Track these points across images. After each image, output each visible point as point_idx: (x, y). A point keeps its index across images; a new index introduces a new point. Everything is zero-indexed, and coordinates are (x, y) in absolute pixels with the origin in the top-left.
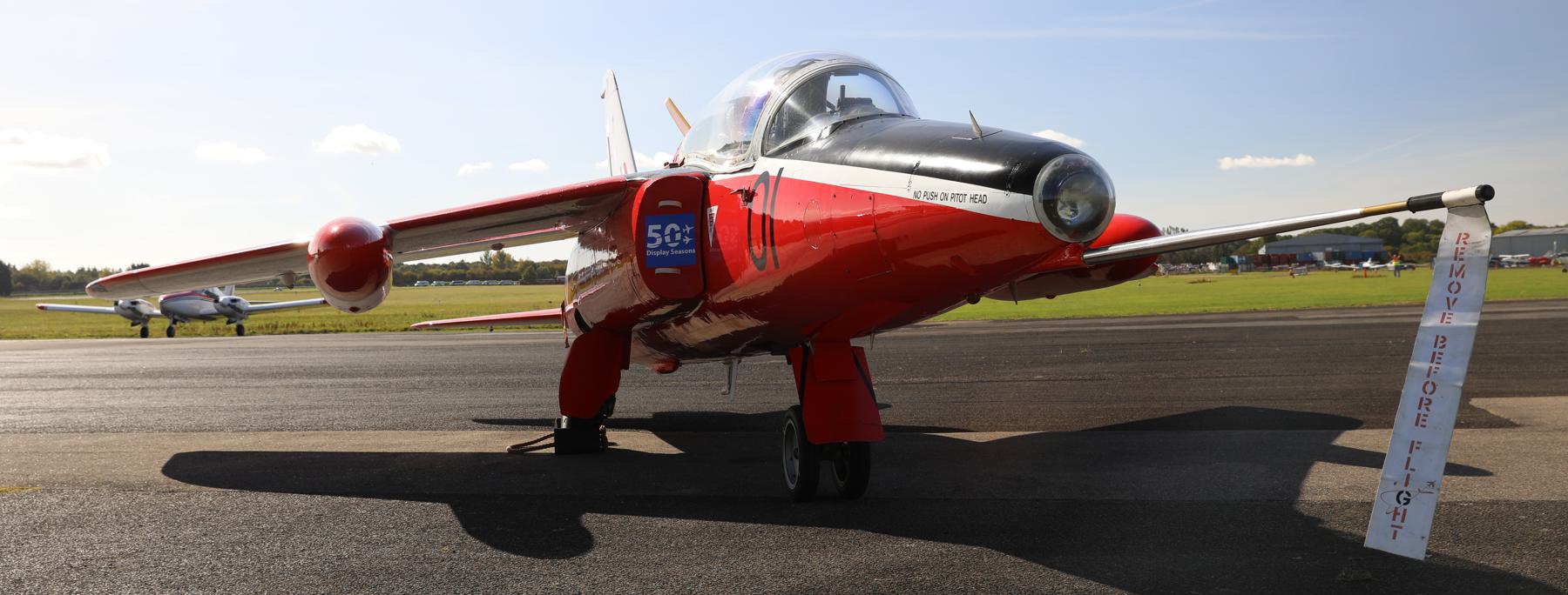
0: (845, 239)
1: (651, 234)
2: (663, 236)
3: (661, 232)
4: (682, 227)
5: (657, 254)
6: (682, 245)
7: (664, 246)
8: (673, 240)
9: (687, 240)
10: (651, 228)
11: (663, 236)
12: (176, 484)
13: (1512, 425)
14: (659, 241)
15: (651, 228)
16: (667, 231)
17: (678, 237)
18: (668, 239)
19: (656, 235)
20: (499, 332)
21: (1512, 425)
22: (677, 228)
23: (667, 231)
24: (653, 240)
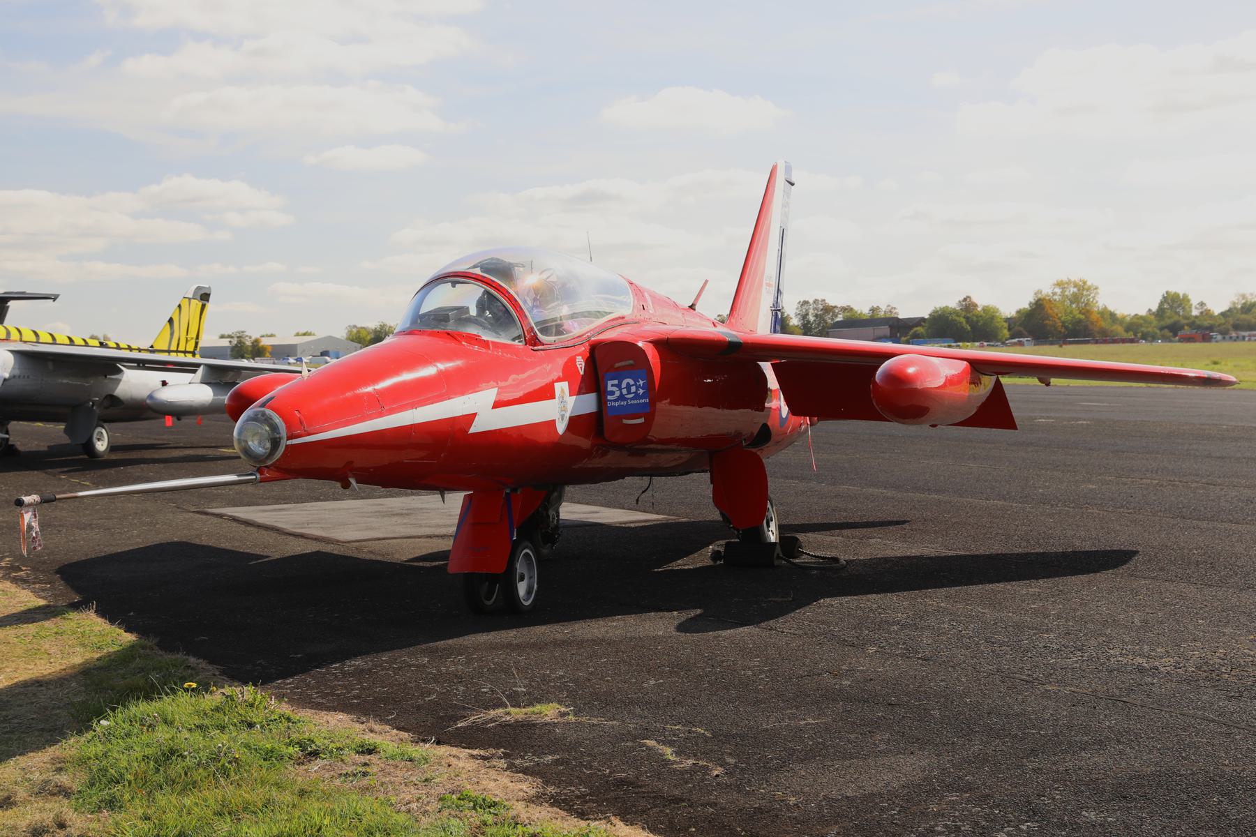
0: (328, 548)
1: (610, 388)
2: (620, 389)
3: (619, 386)
4: (636, 381)
5: (617, 404)
6: (637, 396)
7: (622, 397)
8: (629, 392)
9: (641, 391)
10: (610, 383)
11: (620, 389)
12: (689, 636)
13: (904, 522)
14: (618, 394)
15: (610, 383)
16: (624, 385)
17: (633, 389)
18: (624, 391)
19: (614, 389)
20: (434, 540)
21: (904, 522)
22: (632, 382)
23: (624, 385)
24: (612, 393)
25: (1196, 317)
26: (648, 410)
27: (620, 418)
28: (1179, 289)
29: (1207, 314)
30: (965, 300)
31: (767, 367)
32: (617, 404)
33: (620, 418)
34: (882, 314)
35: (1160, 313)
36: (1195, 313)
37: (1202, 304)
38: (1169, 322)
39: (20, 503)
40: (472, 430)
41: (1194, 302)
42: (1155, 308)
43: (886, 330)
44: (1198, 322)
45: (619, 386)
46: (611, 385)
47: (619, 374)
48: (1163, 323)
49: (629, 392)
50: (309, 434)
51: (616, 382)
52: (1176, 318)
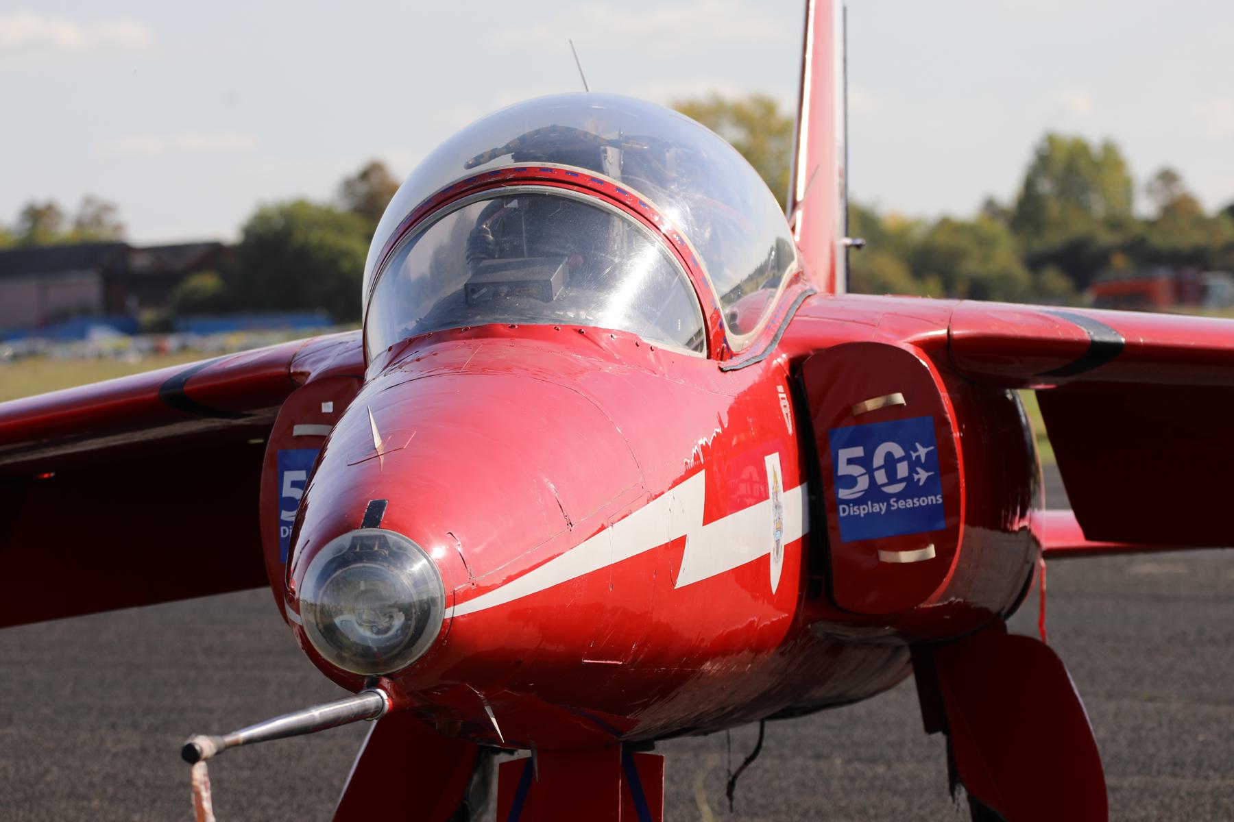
1: (843, 469)
2: (870, 471)
3: (865, 461)
4: (908, 447)
5: (862, 511)
7: (873, 492)
8: (892, 479)
9: (922, 476)
10: (844, 454)
11: (870, 471)
14: (863, 483)
15: (844, 454)
16: (878, 460)
17: (902, 470)
18: (881, 477)
19: (856, 470)
22: (898, 452)
23: (878, 460)
24: (851, 481)
25: (1151, 224)
26: (942, 525)
27: (871, 547)
28: (1086, 121)
29: (1179, 208)
30: (365, 175)
31: (1027, 402)
32: (862, 511)
33: (871, 547)
34: (65, 230)
35: (1027, 213)
36: (1145, 207)
37: (1168, 177)
38: (1054, 239)
39: (191, 755)
40: (682, 581)
41: (1142, 165)
42: (1007, 190)
43: (85, 287)
44: (1157, 241)
45: (865, 461)
46: (845, 460)
47: (867, 432)
48: (1038, 245)
49: (892, 479)
50: (481, 591)
51: (858, 452)
52: (1078, 227)
